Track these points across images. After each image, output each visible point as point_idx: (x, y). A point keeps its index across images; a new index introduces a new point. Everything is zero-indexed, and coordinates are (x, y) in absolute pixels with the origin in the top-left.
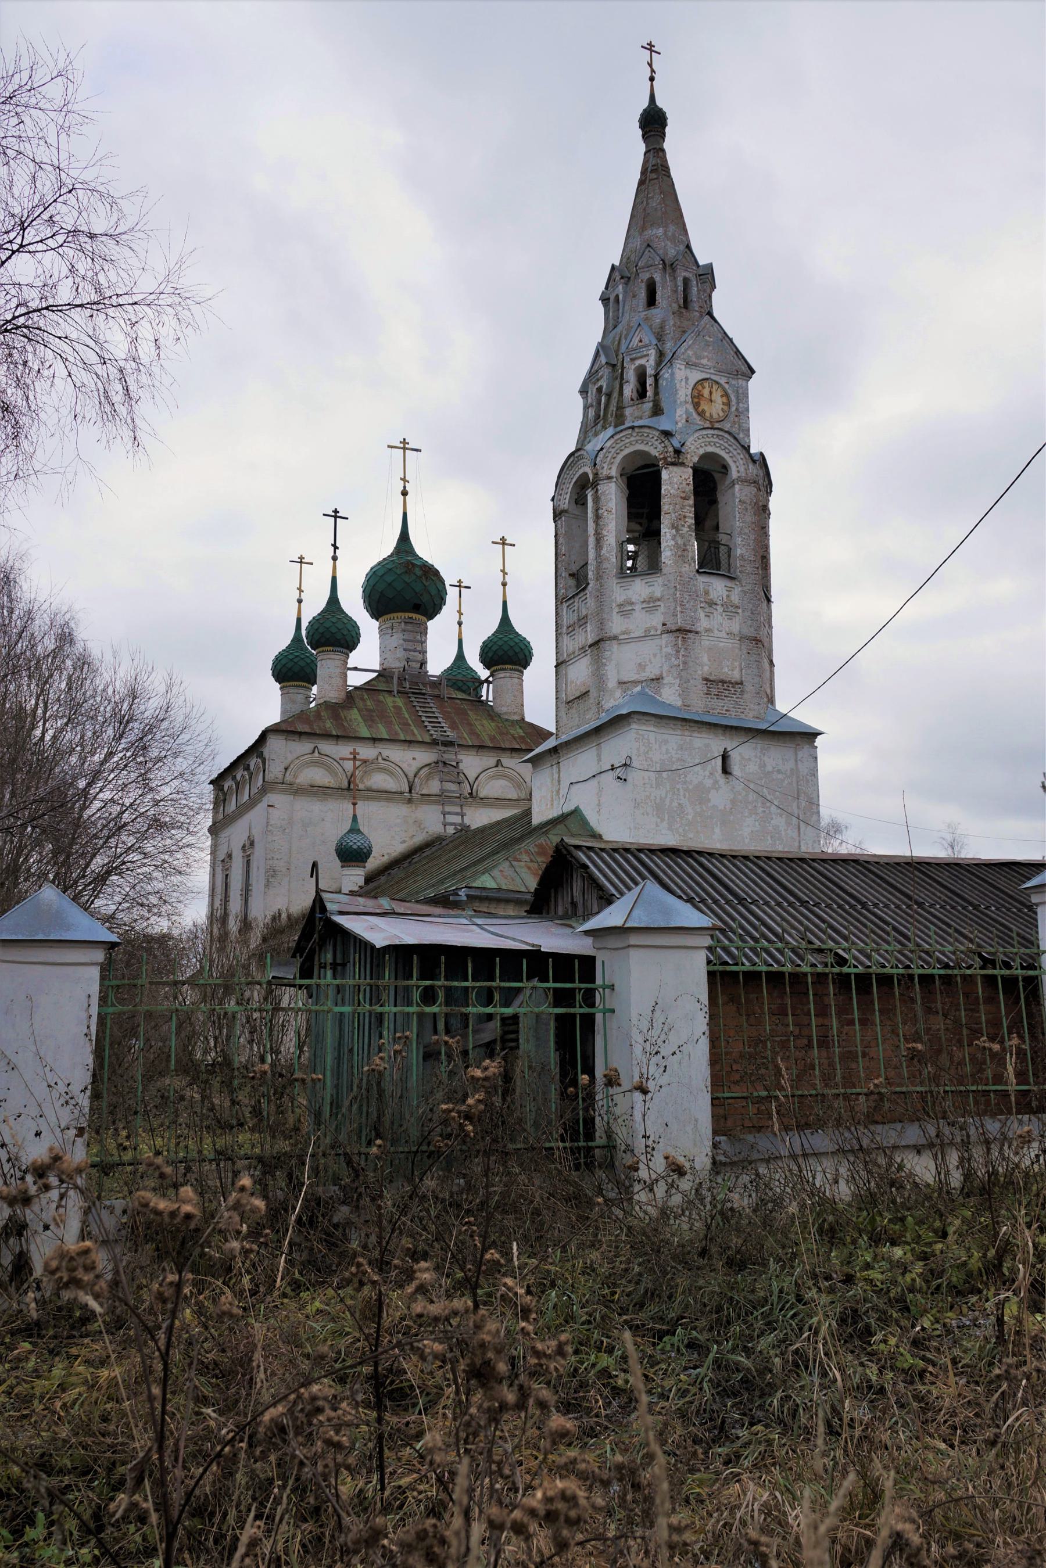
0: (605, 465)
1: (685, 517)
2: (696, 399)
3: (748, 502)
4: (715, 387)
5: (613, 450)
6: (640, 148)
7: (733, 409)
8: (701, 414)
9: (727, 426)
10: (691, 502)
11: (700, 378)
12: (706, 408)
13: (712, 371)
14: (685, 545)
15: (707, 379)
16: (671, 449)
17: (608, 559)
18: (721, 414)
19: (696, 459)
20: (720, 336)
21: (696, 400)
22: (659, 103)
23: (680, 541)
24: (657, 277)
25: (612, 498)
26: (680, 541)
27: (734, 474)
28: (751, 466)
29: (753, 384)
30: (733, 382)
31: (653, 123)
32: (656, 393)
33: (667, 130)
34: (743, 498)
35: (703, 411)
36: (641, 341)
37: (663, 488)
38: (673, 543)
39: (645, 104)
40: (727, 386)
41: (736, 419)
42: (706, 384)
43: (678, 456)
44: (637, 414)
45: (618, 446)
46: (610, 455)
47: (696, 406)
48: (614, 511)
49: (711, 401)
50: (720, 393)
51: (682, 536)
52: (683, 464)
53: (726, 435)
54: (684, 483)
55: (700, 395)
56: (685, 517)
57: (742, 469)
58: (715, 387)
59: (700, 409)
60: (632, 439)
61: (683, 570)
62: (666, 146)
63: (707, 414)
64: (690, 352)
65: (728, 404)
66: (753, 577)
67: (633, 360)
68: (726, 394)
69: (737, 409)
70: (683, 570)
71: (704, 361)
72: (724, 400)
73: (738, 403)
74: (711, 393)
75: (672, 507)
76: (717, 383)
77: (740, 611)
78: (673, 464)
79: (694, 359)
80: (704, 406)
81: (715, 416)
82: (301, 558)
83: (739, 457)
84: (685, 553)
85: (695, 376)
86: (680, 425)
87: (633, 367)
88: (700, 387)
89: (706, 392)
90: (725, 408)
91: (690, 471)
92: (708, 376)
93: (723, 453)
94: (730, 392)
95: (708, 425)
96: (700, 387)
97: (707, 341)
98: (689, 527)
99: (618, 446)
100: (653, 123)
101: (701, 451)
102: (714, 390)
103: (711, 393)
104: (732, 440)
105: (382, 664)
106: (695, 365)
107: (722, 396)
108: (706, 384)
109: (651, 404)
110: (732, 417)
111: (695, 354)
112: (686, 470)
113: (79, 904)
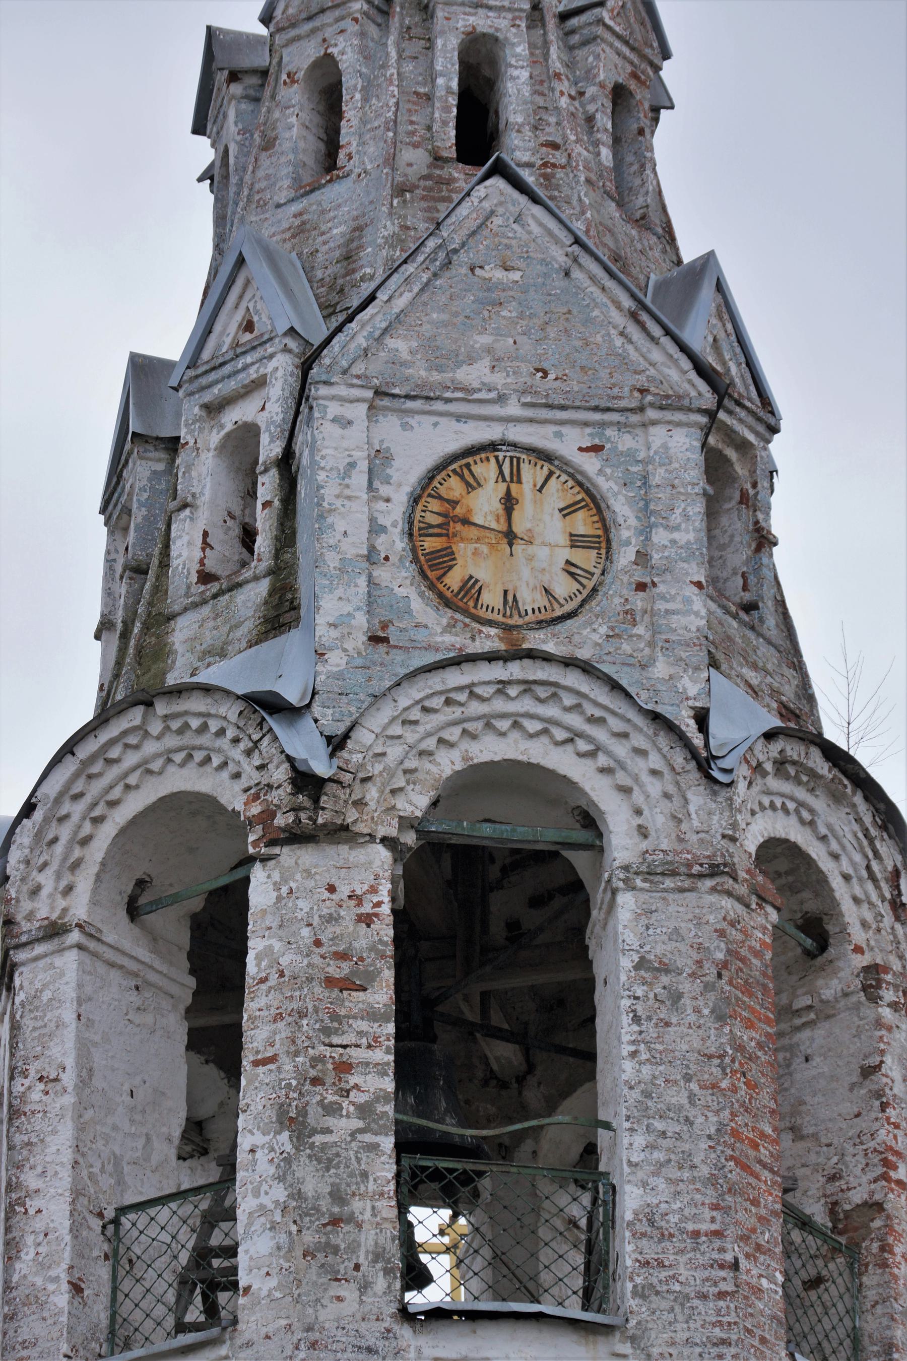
0: (46, 880)
1: (344, 1067)
2: (433, 540)
3: (685, 961)
4: (531, 474)
5: (77, 809)
7: (625, 557)
8: (462, 602)
9: (587, 638)
10: (382, 995)
11: (454, 445)
12: (483, 572)
13: (513, 409)
14: (337, 1197)
15: (492, 446)
16: (280, 774)
17: (36, 1300)
18: (563, 587)
19: (416, 802)
20: (559, 256)
21: (430, 544)
23: (314, 1184)
24: (347, 56)
25: (321, 918)
26: (314, 1184)
27: (622, 845)
28: (698, 798)
29: (776, 437)
30: (626, 442)
32: (286, 537)
34: (659, 949)
35: (471, 588)
36: (249, 326)
37: (255, 945)
38: (280, 1193)
40: (590, 465)
41: (639, 601)
43: (312, 811)
44: (210, 637)
45: (97, 787)
46: (65, 833)
47: (432, 568)
48: (69, 1079)
49: (510, 537)
50: (558, 493)
51: (326, 1160)
52: (341, 833)
53: (573, 679)
54: (348, 914)
55: (454, 520)
56: (344, 1067)
57: (658, 819)
58: (531, 474)
59: (454, 579)
60: (150, 747)
61: (328, 1314)
63: (491, 598)
64: (399, 345)
65: (603, 541)
66: (707, 1310)
67: (214, 409)
68: (592, 500)
69: (642, 557)
70: (328, 1314)
71: (474, 374)
72: (582, 523)
73: (646, 531)
74: (509, 503)
75: (283, 1029)
76: (543, 456)
78: (296, 837)
79: (420, 372)
80: (473, 562)
81: (530, 599)
83: (640, 766)
84: (340, 1238)
85: (423, 442)
86: (336, 660)
87: (215, 438)
88: (453, 487)
89: (484, 505)
90: (586, 559)
91: (382, 855)
93: (562, 762)
94: (606, 485)
95: (489, 640)
96: (453, 487)
97: (488, 285)
98: (364, 1110)
99: (97, 787)
101: (448, 764)
102: (526, 491)
103: (509, 503)
104: (601, 694)
106: (425, 395)
107: (567, 511)
108: (486, 470)
109: (264, 586)
110: (617, 594)
111: (429, 346)
112: (358, 855)
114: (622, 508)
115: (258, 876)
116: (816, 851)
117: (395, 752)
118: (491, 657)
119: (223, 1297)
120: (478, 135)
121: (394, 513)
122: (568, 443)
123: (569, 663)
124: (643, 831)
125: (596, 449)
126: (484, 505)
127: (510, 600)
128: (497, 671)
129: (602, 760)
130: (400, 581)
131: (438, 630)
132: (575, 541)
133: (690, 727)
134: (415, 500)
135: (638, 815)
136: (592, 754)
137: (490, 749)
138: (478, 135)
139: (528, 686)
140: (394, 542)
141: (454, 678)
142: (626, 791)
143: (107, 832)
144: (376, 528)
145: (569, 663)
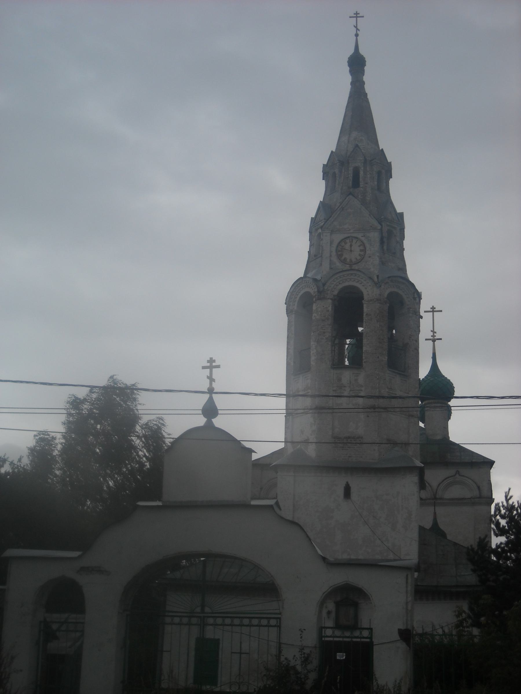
6: (348, 79)
8: (344, 261)
13: (352, 231)
15: (349, 237)
18: (359, 258)
19: (336, 292)
21: (339, 253)
22: (362, 51)
25: (323, 308)
27: (366, 297)
31: (357, 63)
33: (366, 68)
35: (345, 259)
39: (352, 51)
40: (363, 239)
42: (348, 241)
47: (339, 256)
49: (351, 251)
56: (324, 333)
58: (354, 241)
62: (365, 78)
63: (348, 260)
65: (364, 250)
68: (363, 244)
72: (362, 248)
74: (351, 246)
76: (356, 238)
77: (363, 389)
78: (319, 299)
82: (433, 308)
85: (338, 238)
87: (316, 234)
88: (343, 244)
89: (347, 246)
90: (362, 253)
91: (330, 301)
92: (349, 235)
95: (347, 267)
100: (357, 63)
101: (340, 287)
103: (351, 246)
105: (285, 439)
107: (359, 246)
108: (348, 241)
113: (372, 640)
114: (367, 246)
115: (314, 305)
116: (400, 292)
117: (332, 286)
118: (348, 270)
119: (213, 382)
120: (356, 183)
121: (334, 249)
122: (359, 236)
123: (358, 270)
124: (368, 294)
125: (364, 236)
126: (347, 246)
127: (351, 261)
128: (348, 272)
129: (363, 284)
130: (335, 259)
131: (339, 265)
132: (361, 251)
133: (376, 279)
134: (337, 246)
135: (369, 291)
136: (361, 283)
137: (347, 284)
138: (356, 183)
139: (352, 274)
140: (334, 253)
141: (341, 274)
142: (366, 288)
143: (298, 299)
144: (331, 252)
145: (358, 270)
